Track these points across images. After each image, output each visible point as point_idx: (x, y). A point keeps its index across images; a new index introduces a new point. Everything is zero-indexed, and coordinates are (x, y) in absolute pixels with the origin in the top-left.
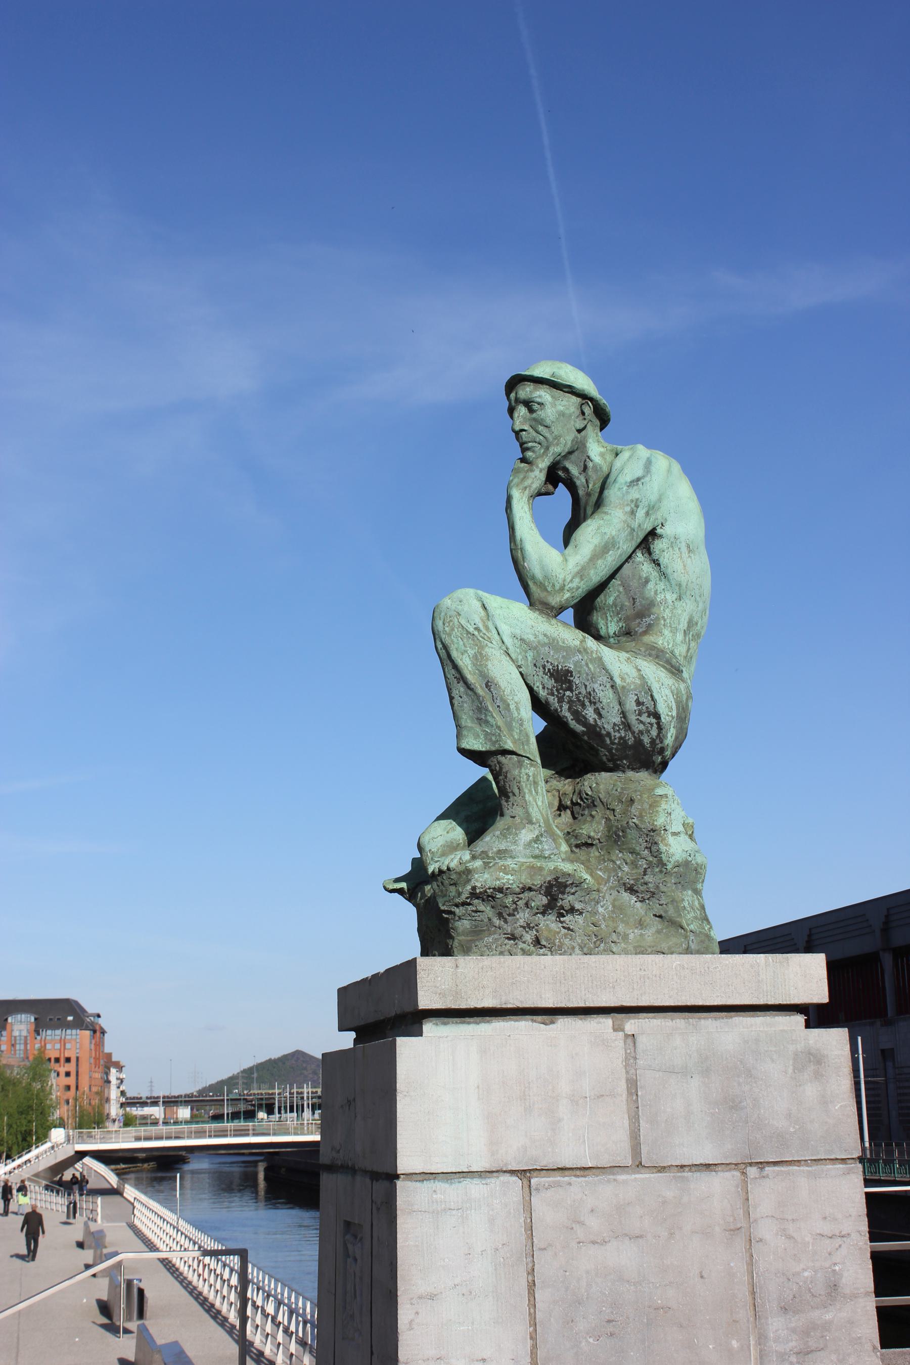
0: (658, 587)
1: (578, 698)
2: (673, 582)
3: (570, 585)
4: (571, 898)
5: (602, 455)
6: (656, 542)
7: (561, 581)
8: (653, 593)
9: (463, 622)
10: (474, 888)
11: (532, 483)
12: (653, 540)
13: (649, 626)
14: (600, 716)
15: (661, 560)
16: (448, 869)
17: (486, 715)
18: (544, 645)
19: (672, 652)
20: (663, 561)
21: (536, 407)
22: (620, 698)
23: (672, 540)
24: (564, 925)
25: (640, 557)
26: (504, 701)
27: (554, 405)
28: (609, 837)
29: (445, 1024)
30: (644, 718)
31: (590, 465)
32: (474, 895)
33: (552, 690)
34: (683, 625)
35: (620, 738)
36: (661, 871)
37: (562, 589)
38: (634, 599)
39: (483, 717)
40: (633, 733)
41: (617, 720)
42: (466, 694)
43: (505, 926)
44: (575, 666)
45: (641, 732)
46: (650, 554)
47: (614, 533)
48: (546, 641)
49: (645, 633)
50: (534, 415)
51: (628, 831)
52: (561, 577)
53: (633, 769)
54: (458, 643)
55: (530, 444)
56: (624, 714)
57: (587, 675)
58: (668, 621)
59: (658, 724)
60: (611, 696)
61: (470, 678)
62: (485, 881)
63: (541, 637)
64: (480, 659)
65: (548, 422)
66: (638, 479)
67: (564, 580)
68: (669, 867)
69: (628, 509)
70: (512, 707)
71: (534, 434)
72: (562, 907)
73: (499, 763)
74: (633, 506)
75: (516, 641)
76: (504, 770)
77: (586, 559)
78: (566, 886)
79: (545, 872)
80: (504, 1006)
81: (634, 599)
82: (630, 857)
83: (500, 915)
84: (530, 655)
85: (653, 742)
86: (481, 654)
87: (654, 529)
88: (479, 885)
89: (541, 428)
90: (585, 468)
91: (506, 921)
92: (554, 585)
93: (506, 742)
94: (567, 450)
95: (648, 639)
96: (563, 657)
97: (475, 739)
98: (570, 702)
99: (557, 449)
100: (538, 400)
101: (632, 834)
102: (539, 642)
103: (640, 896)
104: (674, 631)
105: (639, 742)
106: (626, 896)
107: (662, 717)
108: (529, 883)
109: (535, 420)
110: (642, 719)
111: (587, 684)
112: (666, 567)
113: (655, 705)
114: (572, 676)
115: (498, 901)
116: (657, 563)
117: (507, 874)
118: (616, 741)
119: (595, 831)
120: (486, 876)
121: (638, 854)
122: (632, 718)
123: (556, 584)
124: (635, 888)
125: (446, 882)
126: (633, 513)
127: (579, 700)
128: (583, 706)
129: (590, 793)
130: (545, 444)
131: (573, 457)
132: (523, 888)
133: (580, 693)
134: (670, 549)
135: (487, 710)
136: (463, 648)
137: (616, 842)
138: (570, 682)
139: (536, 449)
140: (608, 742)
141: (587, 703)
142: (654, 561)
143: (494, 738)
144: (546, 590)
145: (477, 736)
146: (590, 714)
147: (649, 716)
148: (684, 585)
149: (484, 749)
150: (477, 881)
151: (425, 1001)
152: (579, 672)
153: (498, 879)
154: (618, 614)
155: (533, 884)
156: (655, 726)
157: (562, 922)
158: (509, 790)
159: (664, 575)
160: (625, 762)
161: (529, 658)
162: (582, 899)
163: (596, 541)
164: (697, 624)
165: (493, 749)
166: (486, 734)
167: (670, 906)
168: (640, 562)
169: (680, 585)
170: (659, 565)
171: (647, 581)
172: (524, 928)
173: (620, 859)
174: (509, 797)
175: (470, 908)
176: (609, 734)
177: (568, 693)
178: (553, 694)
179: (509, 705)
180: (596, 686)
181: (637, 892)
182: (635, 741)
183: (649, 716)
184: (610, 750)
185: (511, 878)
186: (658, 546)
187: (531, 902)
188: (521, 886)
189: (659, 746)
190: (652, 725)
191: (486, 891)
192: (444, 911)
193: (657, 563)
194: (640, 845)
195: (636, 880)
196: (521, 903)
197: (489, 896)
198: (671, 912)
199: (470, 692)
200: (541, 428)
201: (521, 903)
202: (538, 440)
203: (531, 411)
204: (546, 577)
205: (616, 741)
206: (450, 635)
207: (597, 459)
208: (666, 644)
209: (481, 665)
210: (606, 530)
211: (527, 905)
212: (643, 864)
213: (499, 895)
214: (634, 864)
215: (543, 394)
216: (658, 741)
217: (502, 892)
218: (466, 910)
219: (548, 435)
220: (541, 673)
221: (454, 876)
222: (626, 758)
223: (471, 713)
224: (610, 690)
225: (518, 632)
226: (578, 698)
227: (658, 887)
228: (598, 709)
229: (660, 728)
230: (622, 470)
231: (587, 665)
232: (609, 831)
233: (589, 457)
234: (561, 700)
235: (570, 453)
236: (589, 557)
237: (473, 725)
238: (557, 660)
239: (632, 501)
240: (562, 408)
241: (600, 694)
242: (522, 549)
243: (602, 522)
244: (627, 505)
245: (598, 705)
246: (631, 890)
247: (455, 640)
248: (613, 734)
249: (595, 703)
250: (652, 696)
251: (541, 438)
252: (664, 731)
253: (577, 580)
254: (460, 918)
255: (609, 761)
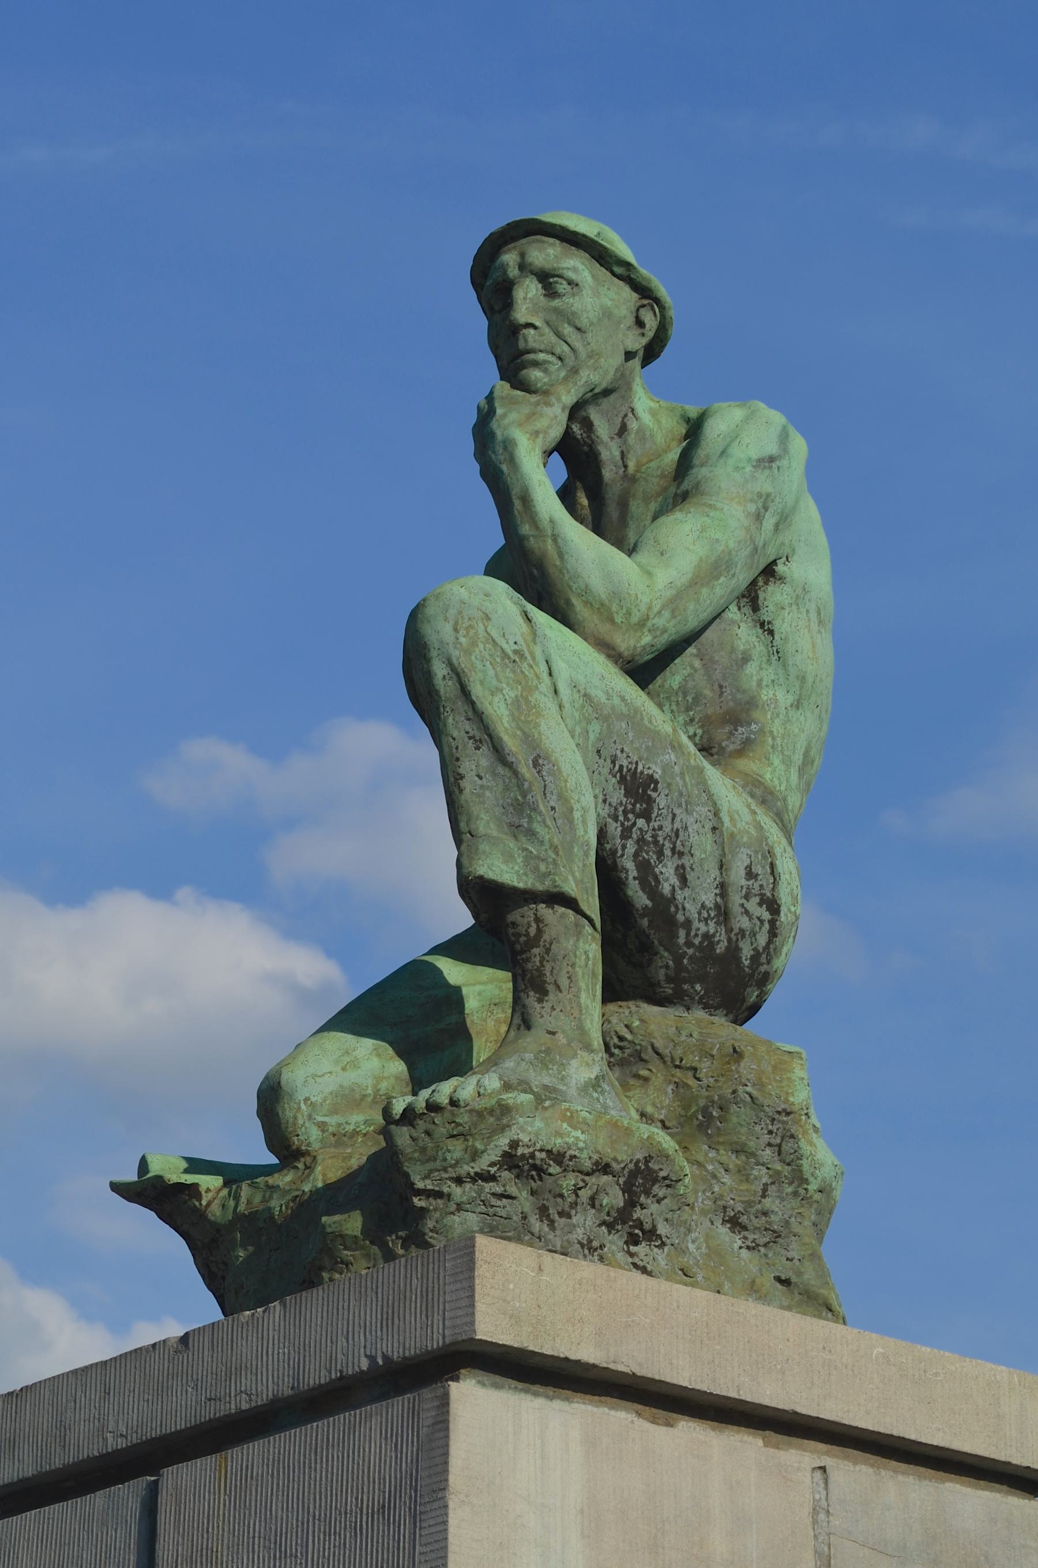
0: (764, 673)
1: (654, 837)
2: (792, 670)
3: (656, 621)
4: (654, 1207)
5: (653, 413)
6: (771, 588)
7: (643, 608)
8: (754, 683)
9: (494, 633)
10: (514, 1144)
11: (550, 427)
12: (766, 583)
13: (747, 744)
14: (684, 881)
15: (776, 626)
16: (454, 1103)
17: (530, 819)
18: (621, 717)
19: (785, 800)
20: (782, 626)
21: (562, 287)
22: (724, 854)
23: (799, 591)
24: (636, 1260)
25: (733, 613)
26: (562, 798)
27: (597, 294)
28: (686, 1120)
29: (497, 1386)
30: (752, 905)
31: (633, 425)
32: (510, 1160)
33: (616, 809)
34: (798, 758)
35: (706, 936)
36: (795, 1194)
37: (642, 624)
38: (721, 687)
39: (524, 822)
40: (729, 930)
41: (709, 898)
42: (494, 774)
43: (551, 1236)
44: (664, 771)
45: (742, 932)
46: (755, 608)
47: (732, 544)
48: (625, 710)
49: (740, 753)
50: (556, 303)
51: (734, 1108)
52: (645, 599)
53: (706, 1007)
54: (484, 672)
55: (542, 356)
56: (723, 888)
57: (681, 794)
58: (779, 741)
59: (773, 923)
60: (709, 848)
61: (511, 743)
62: (537, 1134)
63: (617, 701)
64: (522, 707)
65: (583, 322)
66: (772, 459)
67: (650, 608)
68: (813, 1187)
69: (752, 508)
70: (577, 815)
71: (554, 339)
72: (639, 1224)
73: (538, 920)
74: (760, 505)
75: (576, 696)
76: (546, 937)
77: (685, 580)
78: (655, 1180)
79: (634, 1141)
80: (612, 1366)
81: (721, 687)
82: (733, 1161)
83: (543, 1212)
84: (595, 728)
85: (755, 958)
86: (527, 702)
87: (774, 562)
88: (525, 1138)
89: (567, 330)
90: (623, 430)
91: (552, 1224)
92: (629, 613)
93: (566, 880)
94: (604, 385)
95: (743, 764)
96: (647, 748)
97: (506, 862)
98: (641, 841)
99: (591, 377)
100: (571, 275)
101: (740, 1115)
102: (613, 708)
103: (751, 1237)
104: (787, 762)
105: (733, 950)
106: (724, 1230)
107: (783, 910)
108: (608, 1153)
109: (557, 311)
110: (747, 905)
111: (677, 811)
112: (785, 640)
113: (775, 883)
114: (655, 790)
115: (549, 1180)
116: (767, 628)
117: (575, 1128)
118: (697, 941)
119: (654, 1105)
120: (538, 1124)
121: (753, 1155)
122: (736, 899)
123: (635, 611)
124: (744, 1219)
125: (442, 1130)
126: (758, 517)
127: (656, 842)
128: (660, 854)
129: (629, 1036)
130: (570, 361)
131: (606, 403)
132: (597, 1163)
133: (661, 828)
134: (794, 607)
135: (535, 809)
136: (494, 682)
137: (703, 1128)
138: (650, 801)
139: (553, 368)
140: (682, 940)
141: (668, 852)
142: (762, 625)
143: (543, 867)
144: (612, 621)
145: (509, 858)
146: (667, 872)
147: (760, 904)
148: (810, 680)
149: (521, 885)
150: (522, 1129)
151: (491, 1327)
152: (669, 785)
153: (559, 1134)
154: (688, 709)
155: (615, 1159)
156: (767, 926)
157: (632, 1255)
158: (549, 978)
159: (777, 654)
160: (698, 987)
161: (592, 737)
162: (669, 1216)
163: (701, 550)
164: (813, 762)
165: (540, 887)
166: (529, 857)
167: (807, 1263)
168: (733, 622)
169: (803, 679)
170: (771, 632)
171: (746, 659)
172: (582, 1245)
173: (712, 1161)
174: (546, 993)
175: (489, 1187)
176: (688, 924)
177: (641, 822)
178: (616, 818)
179: (571, 810)
180: (691, 820)
181: (744, 1228)
182: (727, 948)
183: (760, 904)
184: (678, 958)
185: (582, 1137)
186: (773, 596)
187: (602, 1195)
188: (595, 1157)
189: (763, 968)
190: (762, 922)
191: (532, 1156)
192: (419, 1193)
193: (767, 628)
194: (758, 1140)
195: (749, 1204)
196: (585, 1194)
197: (534, 1167)
198: (809, 1276)
199: (501, 770)
200: (567, 330)
201: (585, 1194)
202: (558, 351)
203: (551, 292)
204: (616, 595)
205: (697, 941)
206: (468, 652)
207: (646, 418)
208: (777, 782)
209: (528, 722)
210: (719, 535)
211: (592, 1201)
212: (761, 1175)
213: (554, 1169)
214: (743, 1174)
215: (577, 265)
216: (763, 959)
217: (559, 1163)
218: (482, 1189)
219: (578, 345)
220: (606, 771)
221: (464, 1118)
222: (702, 979)
223: (498, 810)
224: (709, 835)
225: (581, 679)
226: (654, 837)
227: (787, 1222)
228: (683, 867)
229: (773, 933)
230: (734, 437)
231: (682, 774)
232: (686, 1107)
233: (633, 410)
234: (626, 833)
235: (607, 392)
236: (689, 576)
237: (504, 836)
238: (633, 753)
239: (760, 495)
240: (609, 303)
241: (694, 839)
242: (555, 538)
243: (708, 521)
244: (752, 500)
245: (686, 861)
246: (735, 1224)
247: (479, 665)
248: (696, 924)
249: (681, 854)
250: (772, 866)
251: (566, 348)
252: (777, 940)
253: (667, 614)
254: (460, 1207)
255: (669, 979)
